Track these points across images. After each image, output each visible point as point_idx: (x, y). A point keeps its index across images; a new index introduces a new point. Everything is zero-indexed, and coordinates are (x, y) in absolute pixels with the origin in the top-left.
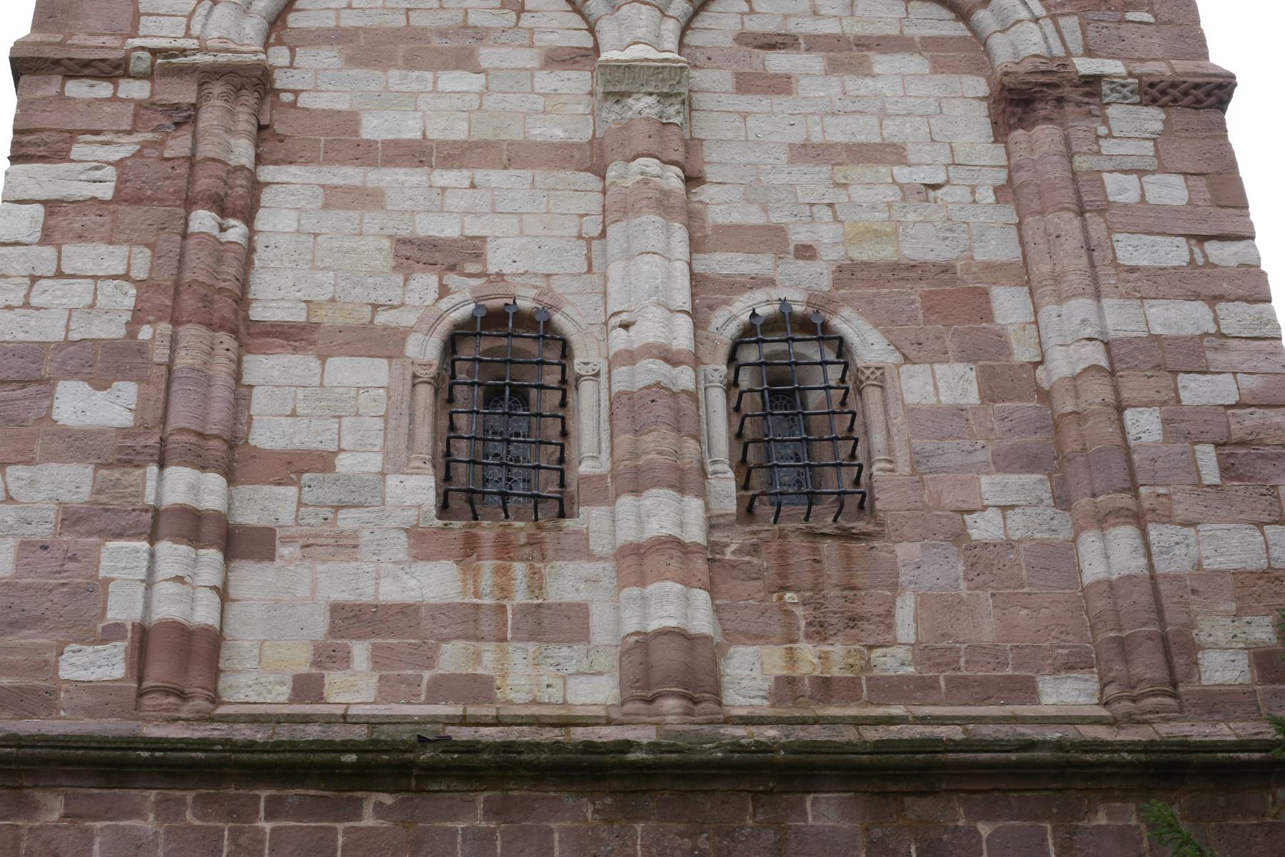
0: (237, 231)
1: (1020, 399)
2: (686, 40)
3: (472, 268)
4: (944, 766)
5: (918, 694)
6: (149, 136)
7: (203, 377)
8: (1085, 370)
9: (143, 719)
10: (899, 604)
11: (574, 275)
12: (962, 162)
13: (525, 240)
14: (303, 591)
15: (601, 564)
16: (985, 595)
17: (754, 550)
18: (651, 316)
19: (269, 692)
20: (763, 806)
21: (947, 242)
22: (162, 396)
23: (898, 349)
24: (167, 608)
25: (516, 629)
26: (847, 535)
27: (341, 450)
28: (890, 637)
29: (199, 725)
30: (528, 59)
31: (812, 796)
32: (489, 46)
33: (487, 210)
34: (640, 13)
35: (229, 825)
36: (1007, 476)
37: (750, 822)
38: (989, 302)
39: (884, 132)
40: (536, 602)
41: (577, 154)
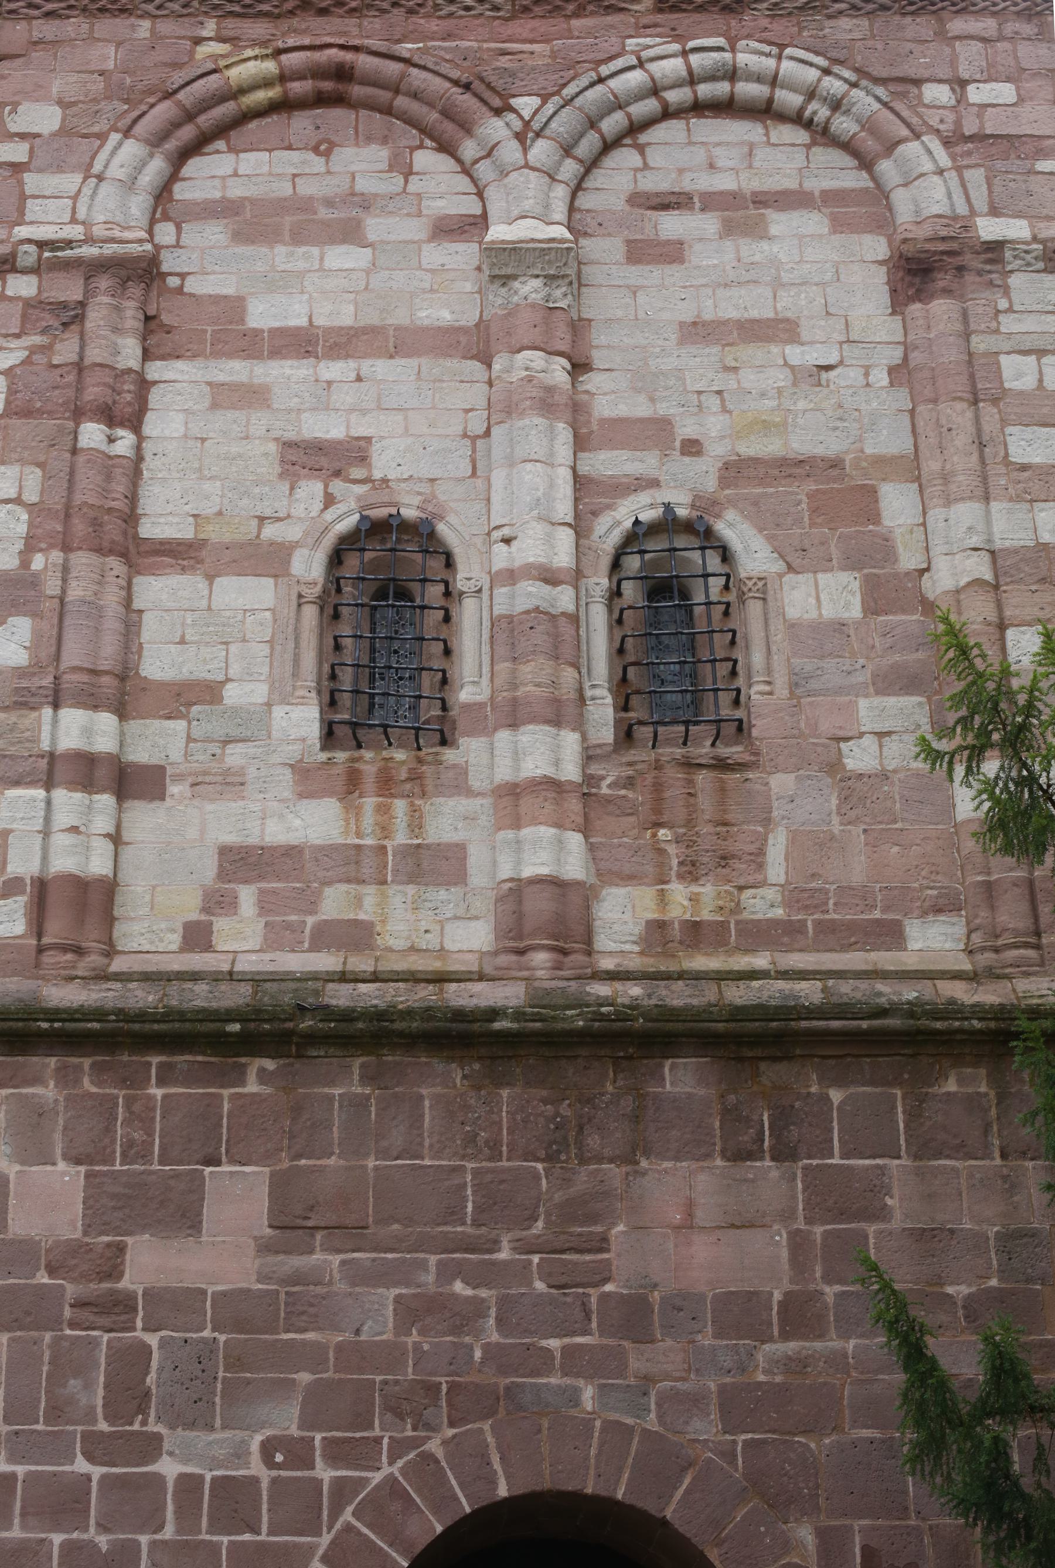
0: (125, 443)
1: (904, 611)
2: (577, 203)
3: (357, 473)
4: (797, 1033)
5: (786, 939)
6: (37, 339)
7: (94, 609)
8: (969, 584)
9: (43, 978)
10: (770, 842)
11: (458, 480)
12: (856, 338)
13: (410, 440)
14: (192, 833)
15: (479, 801)
16: (857, 830)
17: (630, 783)
18: (531, 532)
19: (161, 940)
20: (623, 1071)
21: (837, 433)
22: (55, 632)
23: (782, 556)
24: (63, 863)
25: (396, 871)
26: (722, 765)
27: (228, 680)
28: (759, 877)
29: (95, 984)
30: (414, 229)
31: (670, 1061)
32: (376, 216)
33: (373, 406)
34: (528, 181)
35: (124, 1092)
36: (886, 699)
37: (610, 1088)
38: (877, 501)
39: (778, 305)
40: (416, 842)
41: (463, 339)
